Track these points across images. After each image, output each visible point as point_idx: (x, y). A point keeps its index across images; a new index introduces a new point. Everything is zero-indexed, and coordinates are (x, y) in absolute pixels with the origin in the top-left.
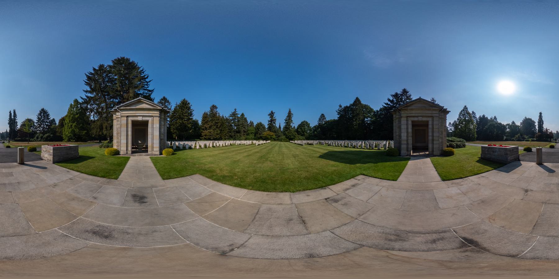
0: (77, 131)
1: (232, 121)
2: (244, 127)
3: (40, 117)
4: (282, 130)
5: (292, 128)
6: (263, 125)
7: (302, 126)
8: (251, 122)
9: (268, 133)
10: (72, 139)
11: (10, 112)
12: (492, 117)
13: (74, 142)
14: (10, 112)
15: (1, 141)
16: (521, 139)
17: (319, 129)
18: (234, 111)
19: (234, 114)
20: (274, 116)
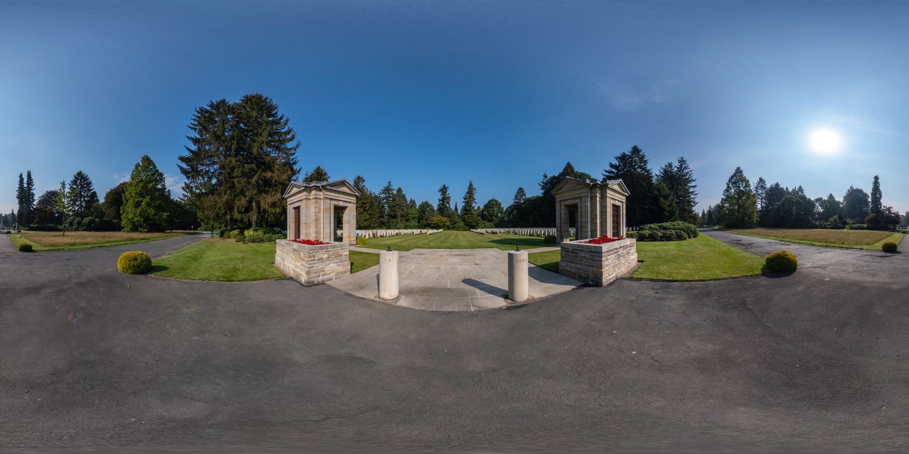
0: (152, 211)
1: (385, 201)
2: (402, 210)
3: (75, 187)
4: (459, 212)
5: (475, 210)
6: (430, 205)
7: (489, 207)
8: (411, 200)
9: (439, 219)
10: (141, 226)
11: (21, 176)
12: (795, 188)
13: (145, 232)
14: (21, 176)
15: (4, 229)
16: (839, 225)
17: (515, 212)
18: (388, 184)
19: (387, 190)
20: (447, 193)
